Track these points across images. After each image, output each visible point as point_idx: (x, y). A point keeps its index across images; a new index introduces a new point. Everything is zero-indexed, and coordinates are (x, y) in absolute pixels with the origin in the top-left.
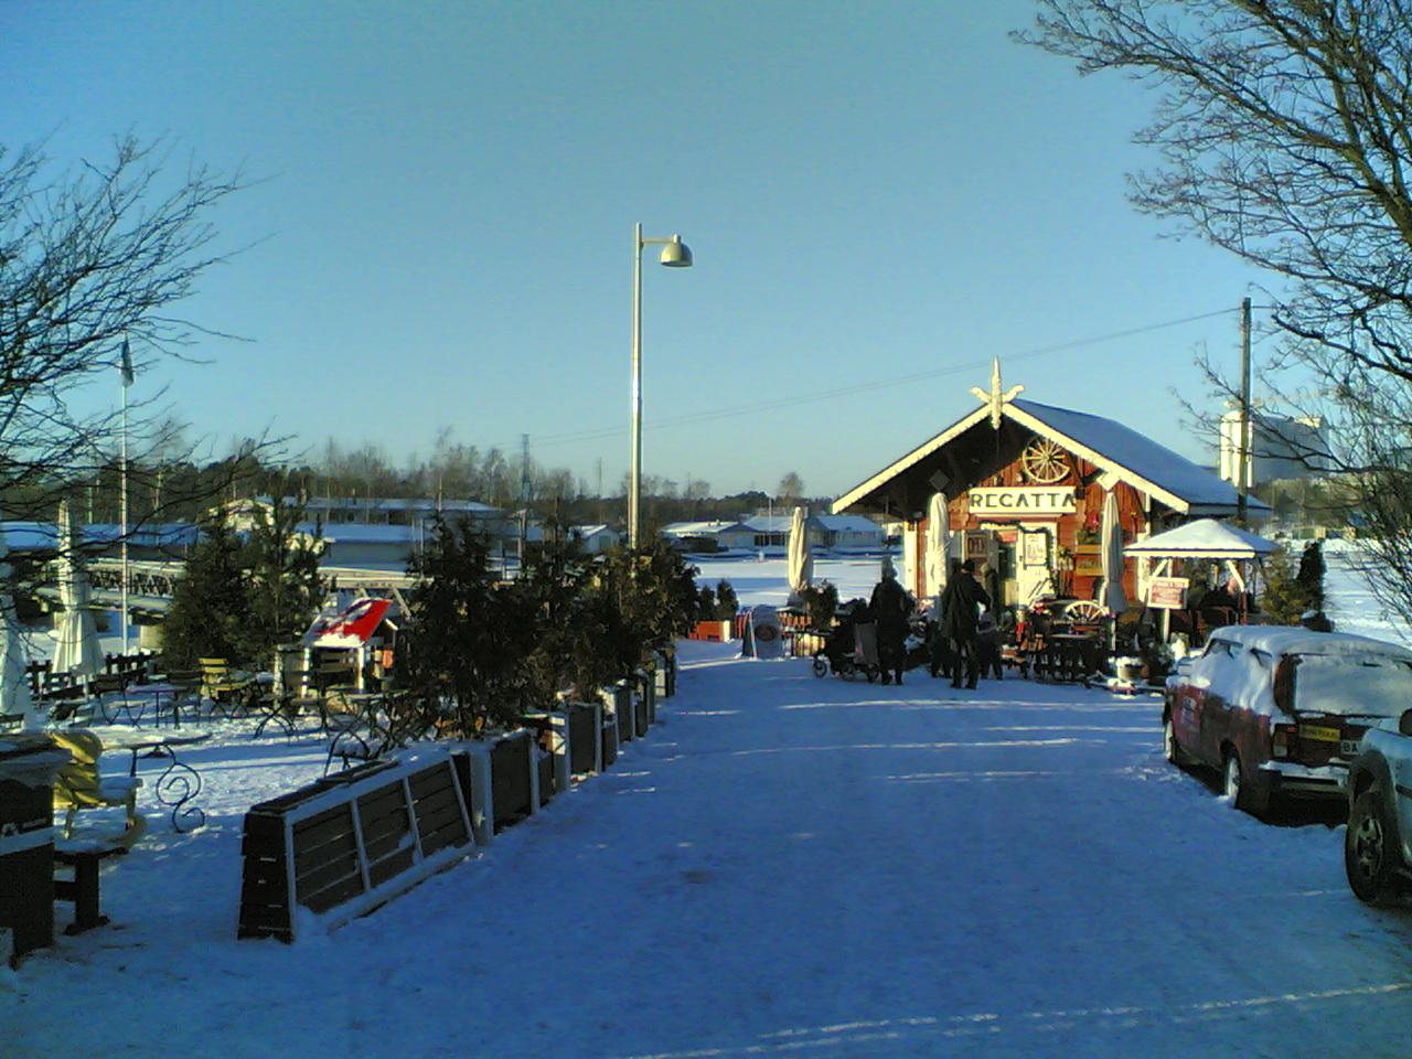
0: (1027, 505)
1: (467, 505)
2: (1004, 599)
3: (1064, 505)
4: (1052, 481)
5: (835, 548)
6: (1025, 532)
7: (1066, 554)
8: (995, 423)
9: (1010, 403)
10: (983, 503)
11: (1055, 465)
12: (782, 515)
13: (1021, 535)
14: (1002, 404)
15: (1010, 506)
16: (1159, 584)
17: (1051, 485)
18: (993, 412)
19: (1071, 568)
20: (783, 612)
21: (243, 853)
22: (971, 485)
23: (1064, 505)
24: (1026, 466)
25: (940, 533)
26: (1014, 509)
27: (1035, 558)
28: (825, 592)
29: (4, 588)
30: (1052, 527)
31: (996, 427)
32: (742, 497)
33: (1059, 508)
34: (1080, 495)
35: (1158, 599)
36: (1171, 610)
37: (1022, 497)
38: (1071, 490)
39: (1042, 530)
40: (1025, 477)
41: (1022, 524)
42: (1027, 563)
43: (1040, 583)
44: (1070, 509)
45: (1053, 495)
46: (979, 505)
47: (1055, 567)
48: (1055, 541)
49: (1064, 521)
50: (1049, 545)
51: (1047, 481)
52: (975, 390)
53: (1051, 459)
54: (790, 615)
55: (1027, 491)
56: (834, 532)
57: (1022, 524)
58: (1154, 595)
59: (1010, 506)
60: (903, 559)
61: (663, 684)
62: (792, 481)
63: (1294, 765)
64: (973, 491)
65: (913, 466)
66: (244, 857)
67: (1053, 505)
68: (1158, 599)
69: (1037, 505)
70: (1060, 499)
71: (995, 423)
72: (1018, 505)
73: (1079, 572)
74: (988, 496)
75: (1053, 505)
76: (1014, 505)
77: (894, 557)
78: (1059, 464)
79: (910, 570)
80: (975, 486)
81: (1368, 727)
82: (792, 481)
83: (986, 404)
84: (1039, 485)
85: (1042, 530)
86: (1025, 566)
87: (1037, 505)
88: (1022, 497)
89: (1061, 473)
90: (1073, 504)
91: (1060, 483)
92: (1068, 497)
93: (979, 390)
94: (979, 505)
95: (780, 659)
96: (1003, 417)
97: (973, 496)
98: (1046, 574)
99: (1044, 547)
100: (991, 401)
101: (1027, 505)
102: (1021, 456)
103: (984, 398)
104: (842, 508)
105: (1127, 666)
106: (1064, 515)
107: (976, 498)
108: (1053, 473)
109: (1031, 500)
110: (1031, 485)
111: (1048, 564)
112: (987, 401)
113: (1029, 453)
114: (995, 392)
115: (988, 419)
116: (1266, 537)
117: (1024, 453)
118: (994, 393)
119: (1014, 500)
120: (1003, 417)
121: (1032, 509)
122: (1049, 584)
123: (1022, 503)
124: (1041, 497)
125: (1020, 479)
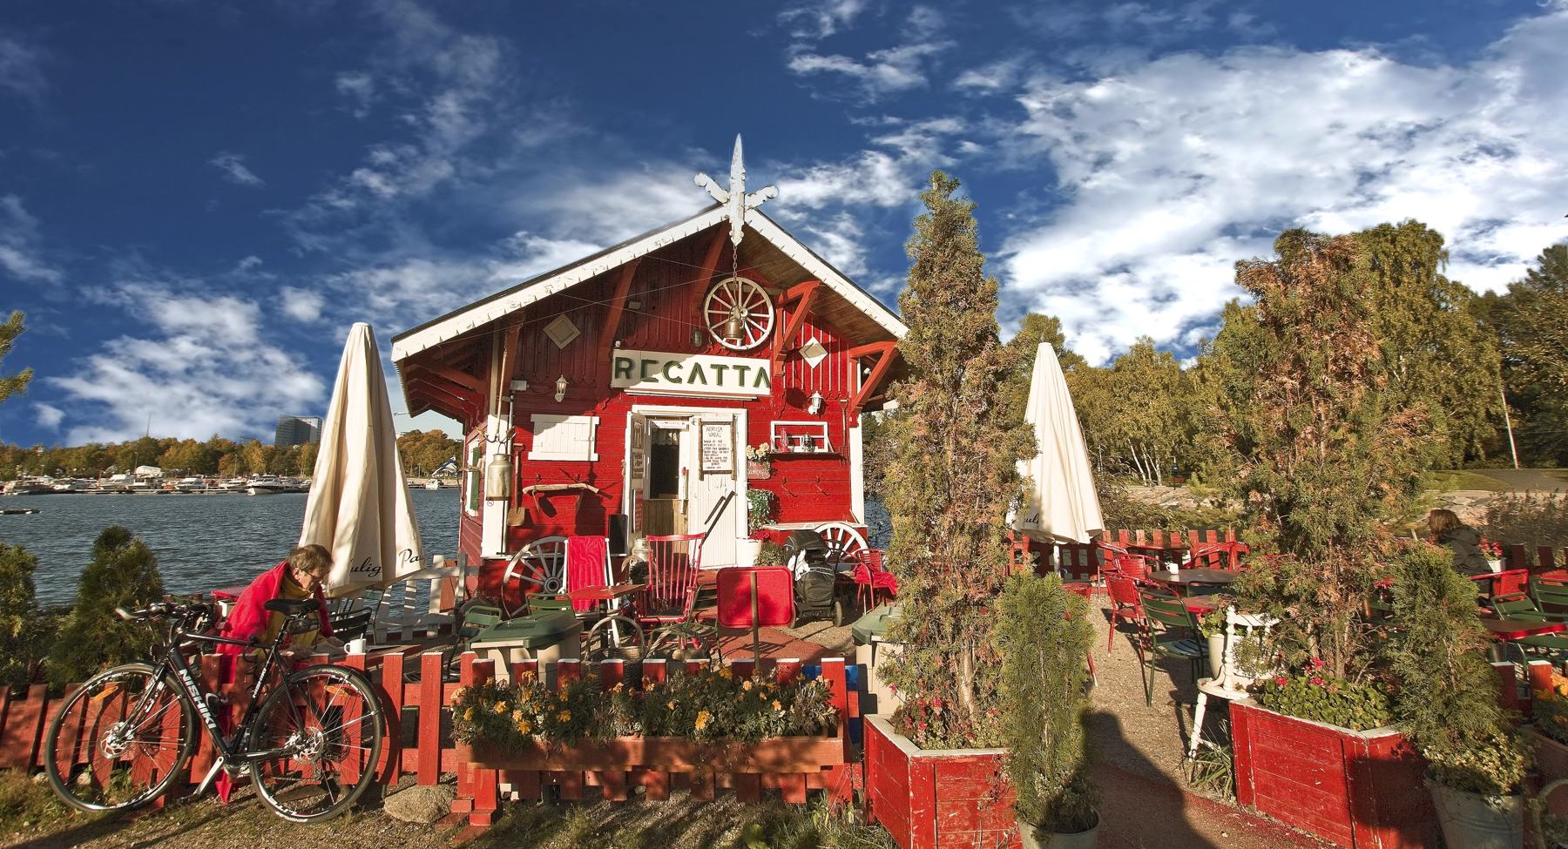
0: (704, 381)
3: (757, 384)
4: (744, 348)
8: (737, 237)
9: (757, 210)
15: (679, 380)
17: (740, 354)
23: (757, 384)
26: (684, 387)
29: (1562, 398)
30: (742, 414)
37: (697, 369)
43: (723, 498)
44: (764, 390)
45: (743, 369)
51: (738, 347)
55: (705, 361)
59: (679, 380)
61: (190, 688)
63: (154, 345)
67: (742, 383)
69: (720, 382)
70: (751, 377)
71: (737, 237)
72: (691, 380)
74: (645, 363)
75: (742, 383)
76: (685, 378)
83: (719, 205)
84: (730, 353)
86: (702, 473)
87: (720, 382)
88: (697, 369)
96: (746, 228)
97: (619, 360)
101: (704, 381)
103: (720, 195)
109: (711, 375)
115: (725, 226)
116: (27, 370)
119: (685, 373)
120: (746, 228)
121: (711, 388)
123: (698, 378)
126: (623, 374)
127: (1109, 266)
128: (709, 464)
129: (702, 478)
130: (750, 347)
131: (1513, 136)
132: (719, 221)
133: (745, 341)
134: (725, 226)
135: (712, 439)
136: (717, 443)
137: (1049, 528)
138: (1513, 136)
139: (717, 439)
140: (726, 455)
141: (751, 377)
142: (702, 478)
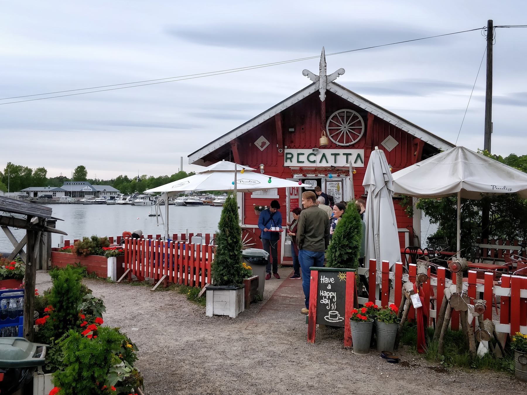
4: (348, 144)
8: (322, 97)
10: (295, 159)
21: (102, 181)
22: (286, 147)
26: (318, 164)
32: (57, 178)
37: (324, 155)
45: (347, 155)
51: (344, 144)
66: (101, 181)
70: (352, 158)
71: (322, 97)
72: (320, 162)
81: (33, 357)
88: (324, 155)
96: (328, 92)
97: (287, 154)
109: (331, 159)
115: (317, 93)
120: (328, 92)
123: (324, 160)
134: (317, 93)
135: (332, 188)
140: (339, 196)
141: (352, 158)
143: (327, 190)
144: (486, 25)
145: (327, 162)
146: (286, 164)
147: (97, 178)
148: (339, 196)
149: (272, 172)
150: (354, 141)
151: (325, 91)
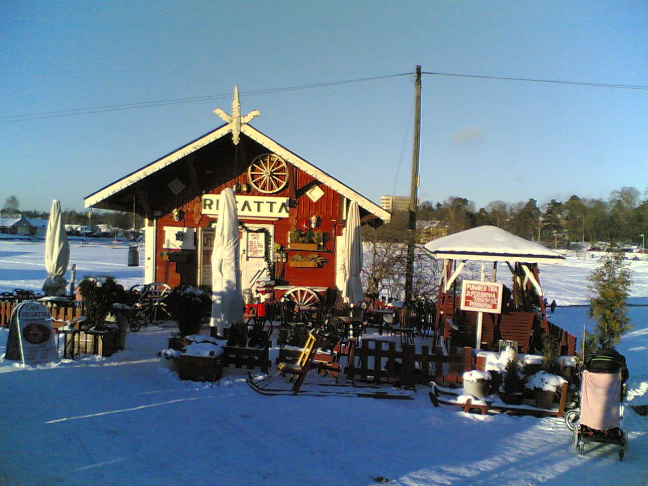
0: (250, 210)
1: (453, 325)
2: (241, 288)
3: (280, 211)
4: (271, 192)
5: (36, 236)
6: (249, 231)
7: (282, 249)
8: (236, 140)
10: (214, 206)
11: (273, 179)
12: (7, 217)
13: (245, 234)
14: (241, 124)
16: (473, 287)
17: (270, 195)
18: (233, 128)
19: (284, 260)
20: (47, 302)
22: (203, 192)
23: (280, 211)
24: (250, 179)
25: (229, 228)
27: (256, 252)
28: (104, 285)
30: (271, 229)
31: (236, 142)
33: (276, 214)
34: (291, 204)
35: (471, 303)
36: (484, 313)
38: (284, 200)
39: (262, 230)
40: (249, 187)
41: (246, 225)
42: (249, 256)
43: (259, 271)
44: (284, 214)
45: (271, 203)
46: (210, 208)
47: (271, 258)
48: (272, 239)
49: (280, 224)
50: (267, 242)
52: (218, 111)
53: (272, 174)
54: (55, 305)
55: (251, 199)
56: (36, 228)
57: (246, 225)
58: (467, 298)
60: (45, 242)
62: (13, 200)
64: (205, 197)
65: (160, 171)
67: (271, 211)
68: (471, 303)
69: (259, 210)
70: (276, 207)
71: (236, 140)
73: (292, 264)
75: (271, 211)
77: (69, 242)
78: (276, 178)
79: (149, 259)
80: (206, 193)
82: (13, 200)
83: (227, 124)
84: (260, 194)
85: (262, 230)
86: (248, 258)
87: (259, 210)
89: (278, 187)
90: (287, 211)
91: (277, 194)
92: (283, 205)
93: (222, 112)
94: (210, 208)
95: (54, 365)
97: (205, 200)
98: (264, 264)
99: (263, 244)
100: (232, 121)
101: (250, 210)
102: (246, 171)
103: (226, 118)
104: (93, 203)
105: (479, 380)
106: (280, 218)
107: (208, 202)
108: (272, 185)
109: (254, 207)
110: (253, 195)
111: (267, 257)
112: (228, 121)
113: (253, 169)
114: (236, 113)
115: (230, 135)
117: (250, 168)
118: (234, 114)
120: (242, 136)
121: (254, 213)
122: (266, 273)
123: (246, 208)
124: (261, 204)
125: (245, 189)
126: (207, 207)
127: (620, 399)
128: (252, 253)
129: (247, 260)
130: (275, 191)
131: (250, 283)
132: (227, 132)
133: (272, 188)
134: (230, 135)
135: (254, 240)
136: (257, 243)
137: (520, 204)
138: (250, 283)
139: (256, 240)
140: (261, 249)
141: (276, 207)
142: (247, 260)
143: (249, 242)
144: (415, 71)
145: (217, 209)
146: (204, 212)
147: (37, 210)
148: (261, 249)
149: (360, 261)
150: (269, 191)
151: (239, 133)
